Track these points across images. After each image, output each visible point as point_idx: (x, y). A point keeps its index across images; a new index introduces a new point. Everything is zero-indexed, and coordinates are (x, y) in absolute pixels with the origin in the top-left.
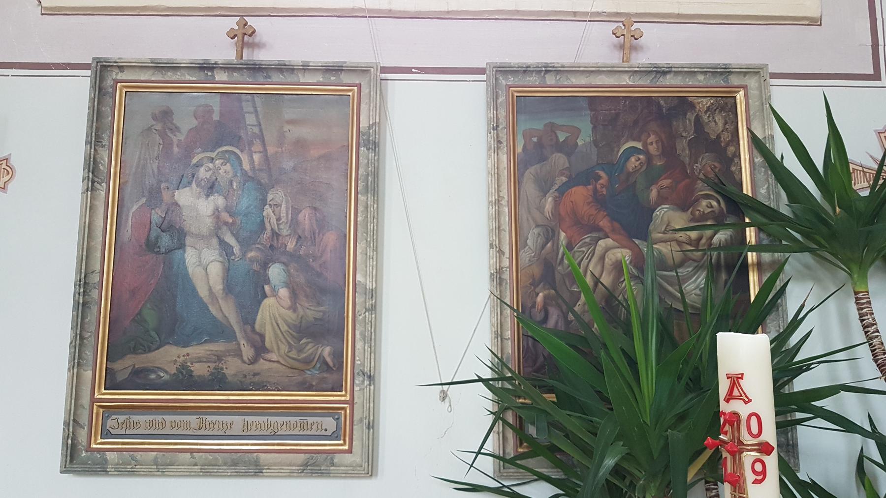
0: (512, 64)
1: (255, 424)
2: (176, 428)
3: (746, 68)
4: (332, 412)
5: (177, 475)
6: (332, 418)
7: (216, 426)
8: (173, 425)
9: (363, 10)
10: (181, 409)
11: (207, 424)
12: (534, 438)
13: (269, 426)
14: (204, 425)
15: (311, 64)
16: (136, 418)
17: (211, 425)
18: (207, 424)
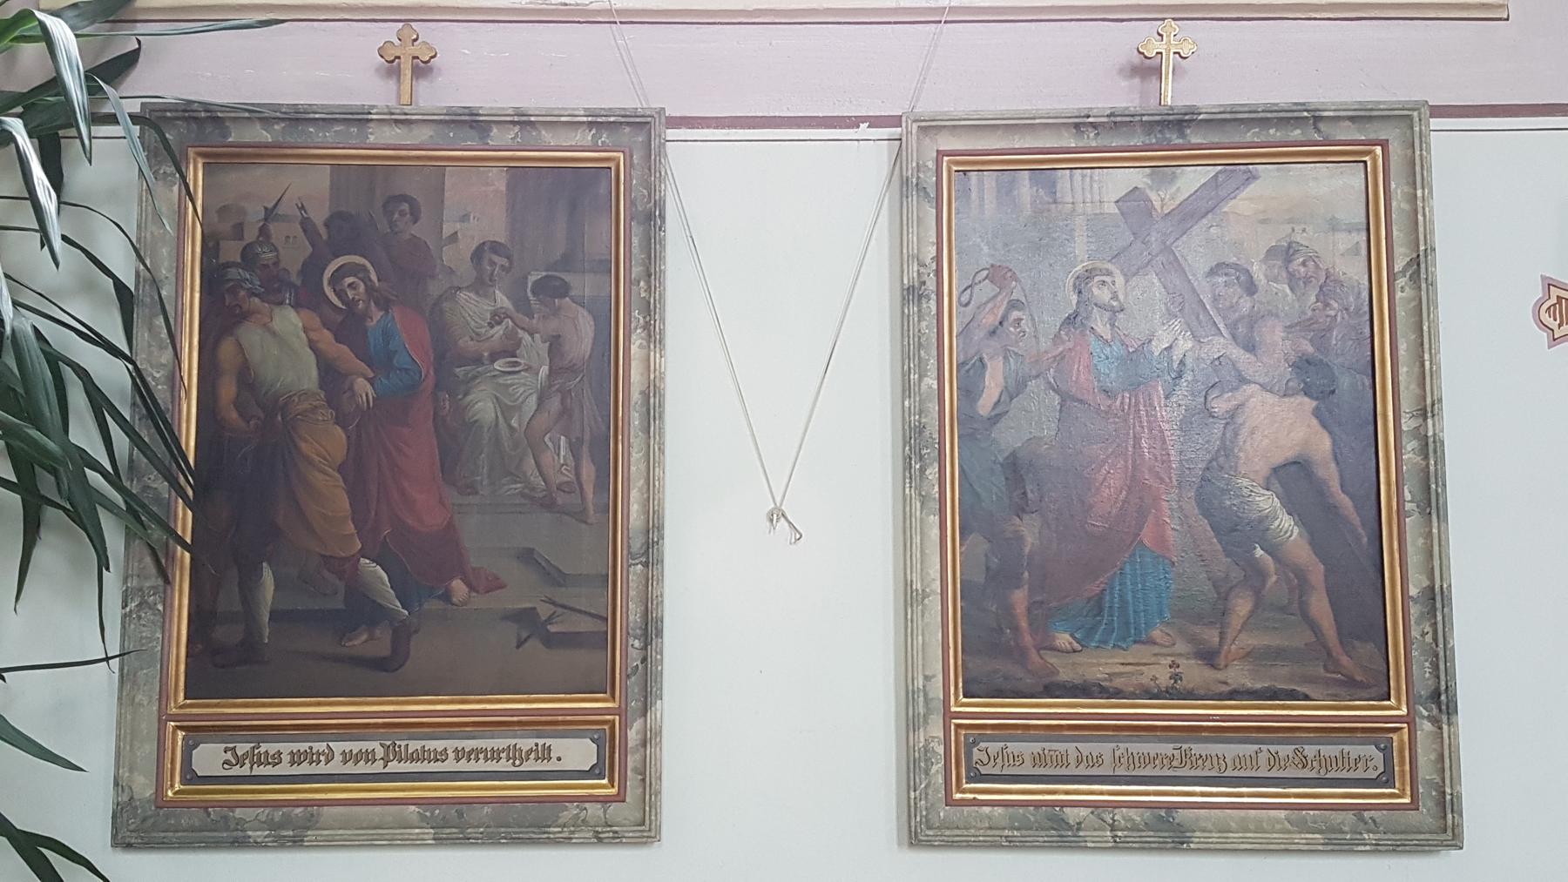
0: (1132, 109)
1: (1160, 757)
2: (354, 752)
3: (1076, 117)
4: (1376, 734)
5: (1345, 851)
6: (1374, 747)
7: (1208, 763)
8: (1326, 762)
9: (609, 12)
10: (1362, 732)
11: (1193, 759)
12: (981, 775)
13: (1147, 761)
14: (1188, 761)
15: (481, 112)
16: (1014, 747)
17: (1200, 762)
18: (1193, 759)
